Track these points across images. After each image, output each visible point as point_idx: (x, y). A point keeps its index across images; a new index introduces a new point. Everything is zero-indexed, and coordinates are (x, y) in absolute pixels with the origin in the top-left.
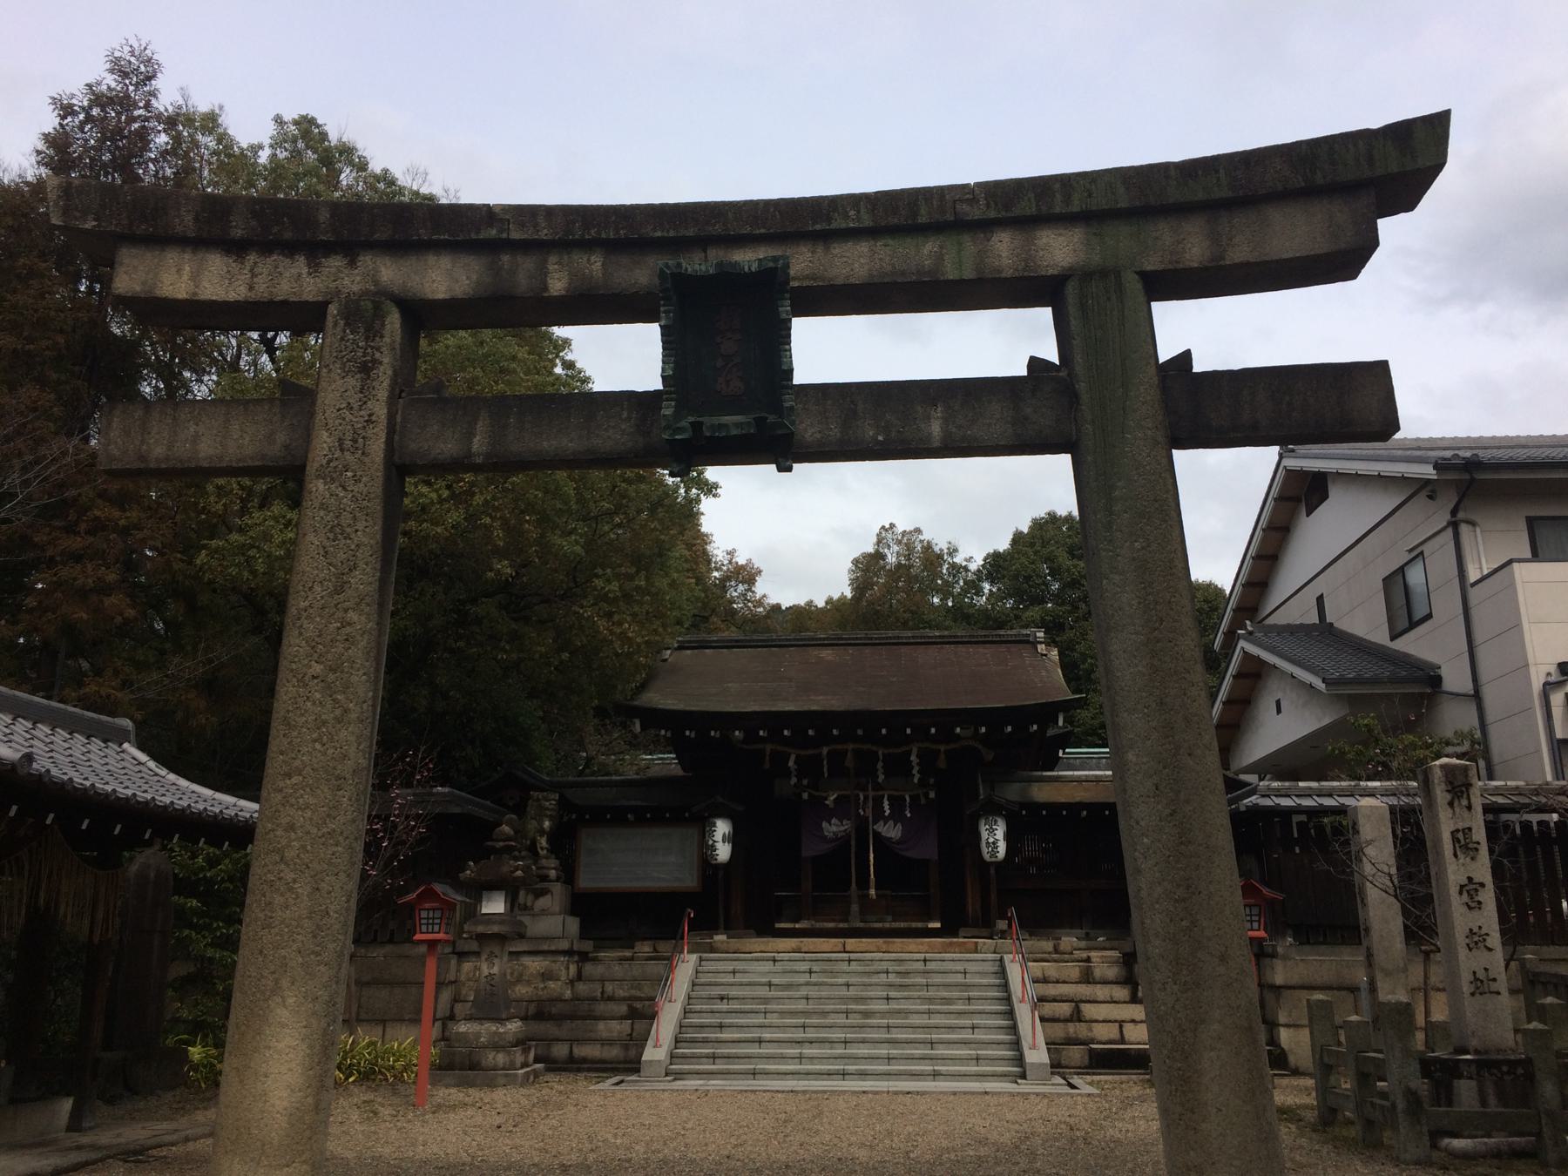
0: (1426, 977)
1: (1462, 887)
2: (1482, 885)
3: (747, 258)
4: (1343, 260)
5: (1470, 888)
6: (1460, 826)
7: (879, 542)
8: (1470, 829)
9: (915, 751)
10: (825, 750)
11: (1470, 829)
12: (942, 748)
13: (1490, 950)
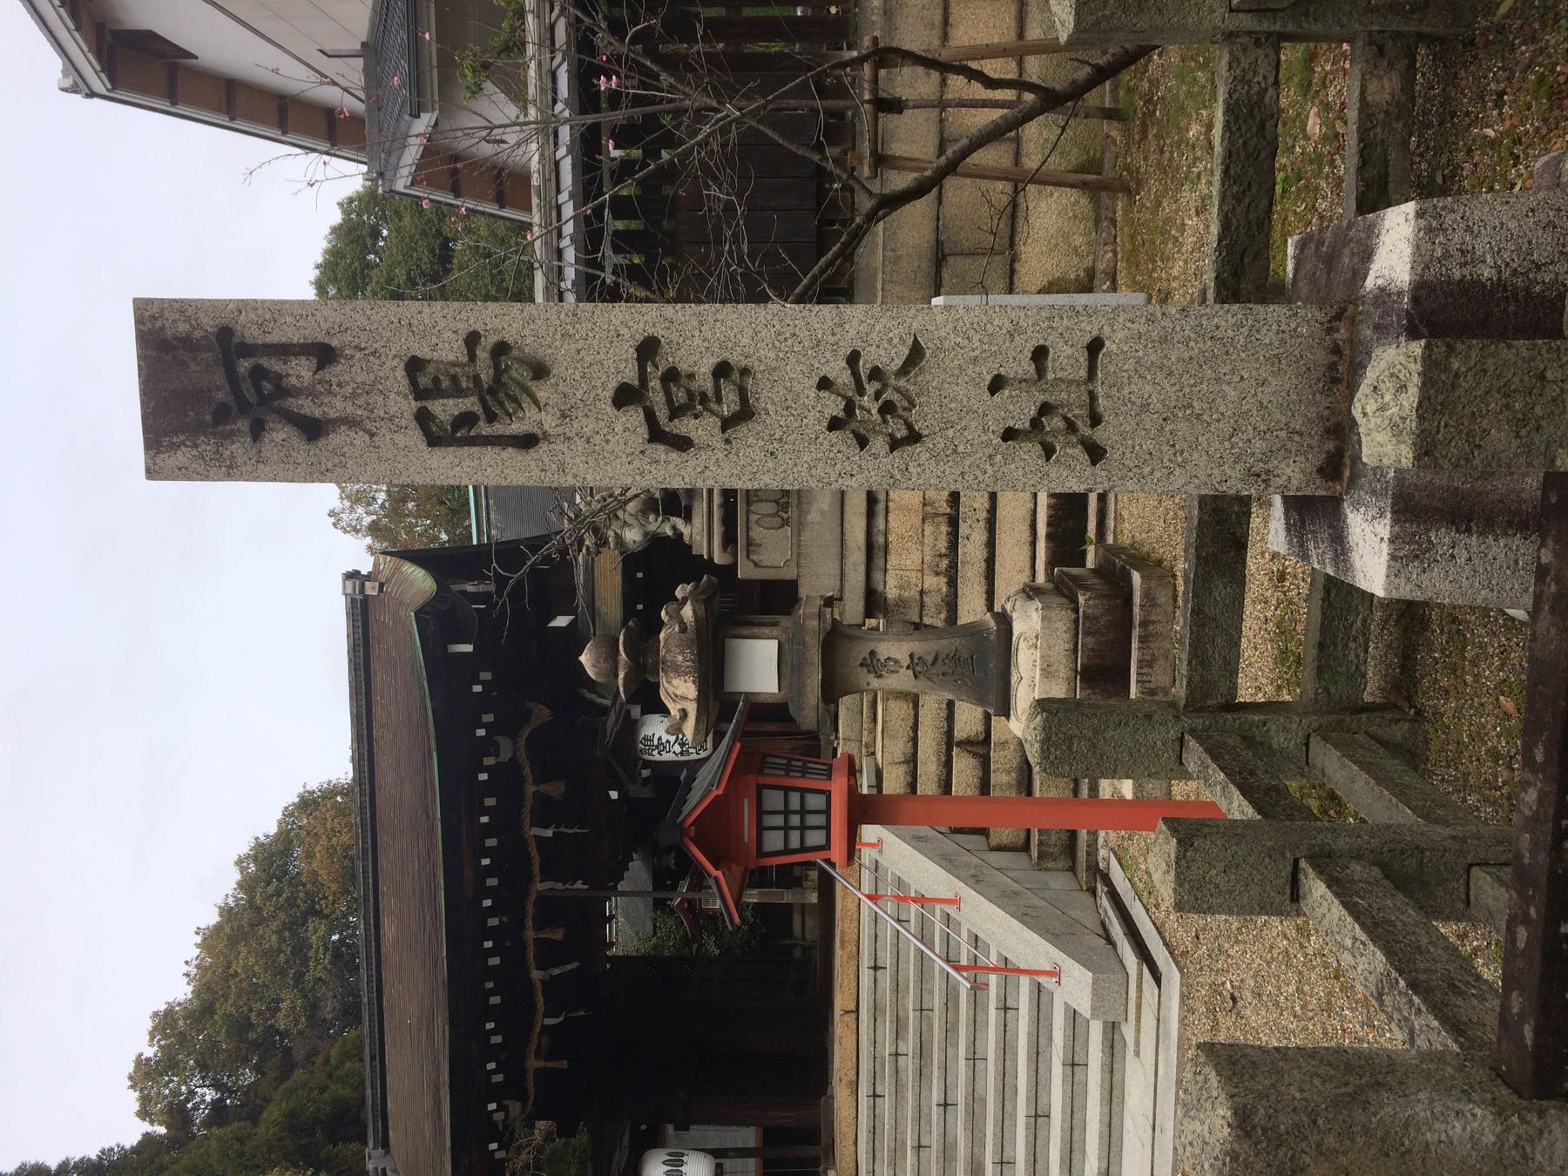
0: (920, 105)
1: (657, 435)
2: (648, 349)
5: (659, 397)
6: (403, 406)
7: (357, 531)
8: (415, 366)
9: (536, 831)
10: (536, 975)
11: (415, 366)
12: (530, 789)
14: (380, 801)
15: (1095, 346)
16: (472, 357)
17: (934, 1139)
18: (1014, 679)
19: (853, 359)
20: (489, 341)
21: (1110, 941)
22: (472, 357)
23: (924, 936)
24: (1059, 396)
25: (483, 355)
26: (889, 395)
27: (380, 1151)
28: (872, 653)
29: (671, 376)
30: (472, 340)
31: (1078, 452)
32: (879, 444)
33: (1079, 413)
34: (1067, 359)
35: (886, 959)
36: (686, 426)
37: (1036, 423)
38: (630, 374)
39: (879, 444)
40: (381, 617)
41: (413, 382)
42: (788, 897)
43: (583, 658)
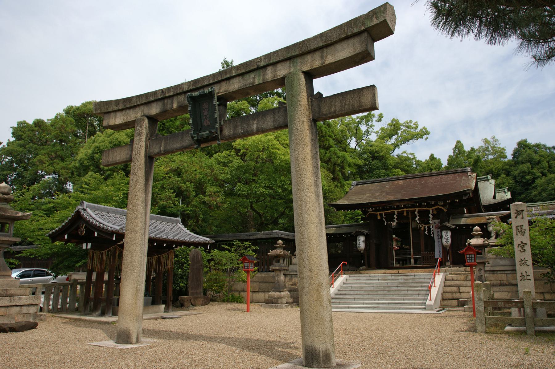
1: (519, 245)
2: (526, 244)
3: (207, 91)
4: (366, 56)
6: (519, 225)
13: (528, 265)
14: (425, 178)
34: (529, 278)
35: (416, 277)
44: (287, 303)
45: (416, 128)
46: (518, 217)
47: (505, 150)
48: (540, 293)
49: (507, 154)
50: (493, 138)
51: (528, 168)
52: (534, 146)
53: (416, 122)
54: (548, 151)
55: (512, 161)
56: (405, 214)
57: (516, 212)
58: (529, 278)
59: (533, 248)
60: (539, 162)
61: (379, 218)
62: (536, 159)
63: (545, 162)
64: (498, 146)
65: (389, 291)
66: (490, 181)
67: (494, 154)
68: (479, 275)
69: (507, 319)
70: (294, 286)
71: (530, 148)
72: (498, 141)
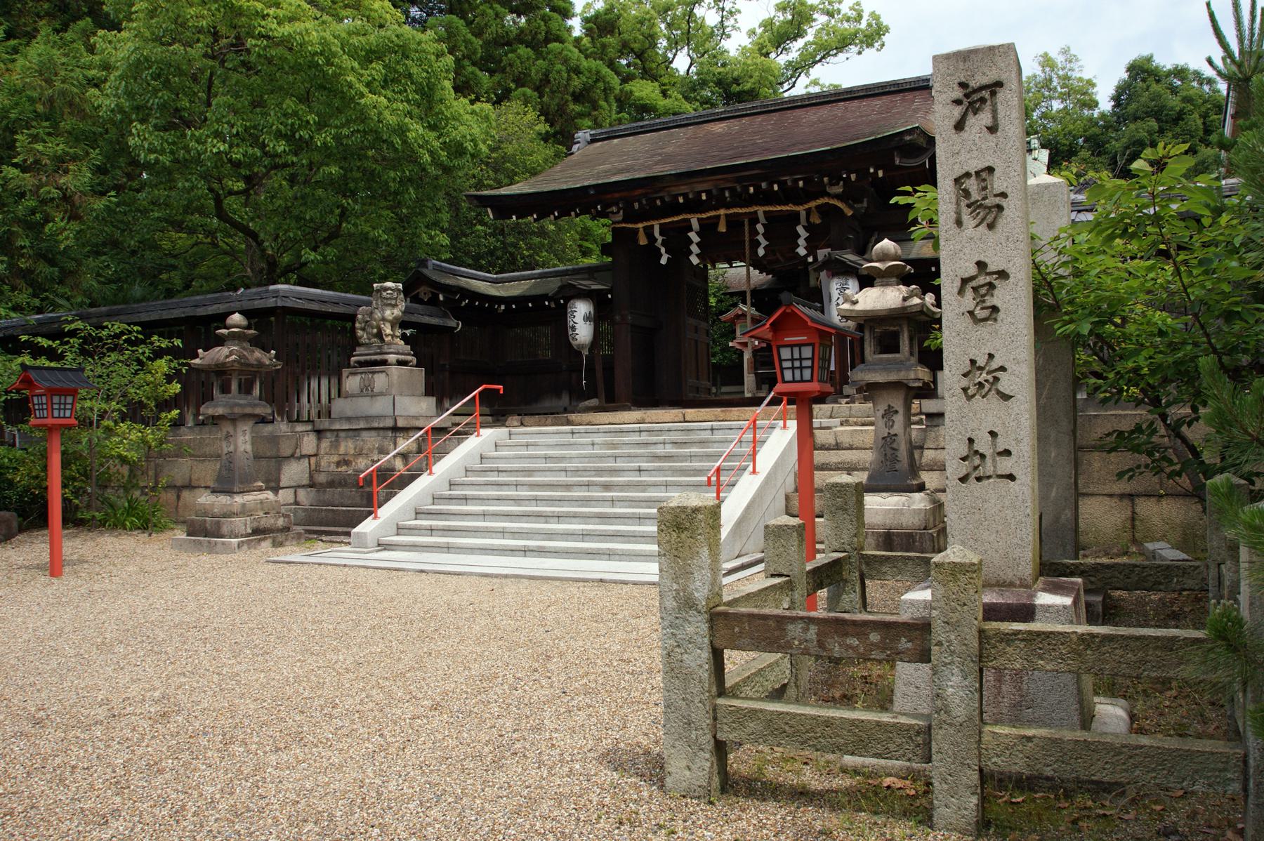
1: (965, 281)
2: (1003, 275)
6: (974, 165)
11: (990, 170)
13: (1006, 397)
14: (798, 112)
15: (1011, 477)
16: (996, 196)
17: (620, 464)
18: (884, 494)
19: (1002, 369)
20: (1004, 203)
21: (738, 556)
22: (996, 196)
23: (730, 456)
24: (989, 461)
25: (997, 200)
26: (987, 386)
27: (589, 138)
28: (896, 412)
29: (991, 286)
30: (1004, 195)
31: (964, 472)
32: (965, 382)
33: (980, 472)
34: (1005, 465)
35: (718, 436)
36: (969, 294)
37: (976, 452)
38: (992, 267)
39: (965, 382)
40: (918, 99)
41: (983, 170)
42: (749, 379)
43: (886, 241)
44: (256, 532)
45: (859, 18)
46: (971, 120)
47: (1094, 85)
48: (1122, 496)
49: (1098, 98)
50: (1065, 51)
51: (1150, 133)
52: (1169, 73)
53: (858, 4)
54: (1206, 88)
55: (1114, 114)
56: (722, 228)
57: (958, 93)
58: (1005, 465)
59: (1046, 306)
60: (1180, 117)
61: (643, 241)
62: (1172, 109)
63: (1196, 115)
64: (1076, 74)
65: (607, 487)
66: (1035, 154)
67: (1063, 98)
68: (885, 432)
69: (828, 723)
70: (344, 468)
71: (1158, 81)
72: (1077, 60)
